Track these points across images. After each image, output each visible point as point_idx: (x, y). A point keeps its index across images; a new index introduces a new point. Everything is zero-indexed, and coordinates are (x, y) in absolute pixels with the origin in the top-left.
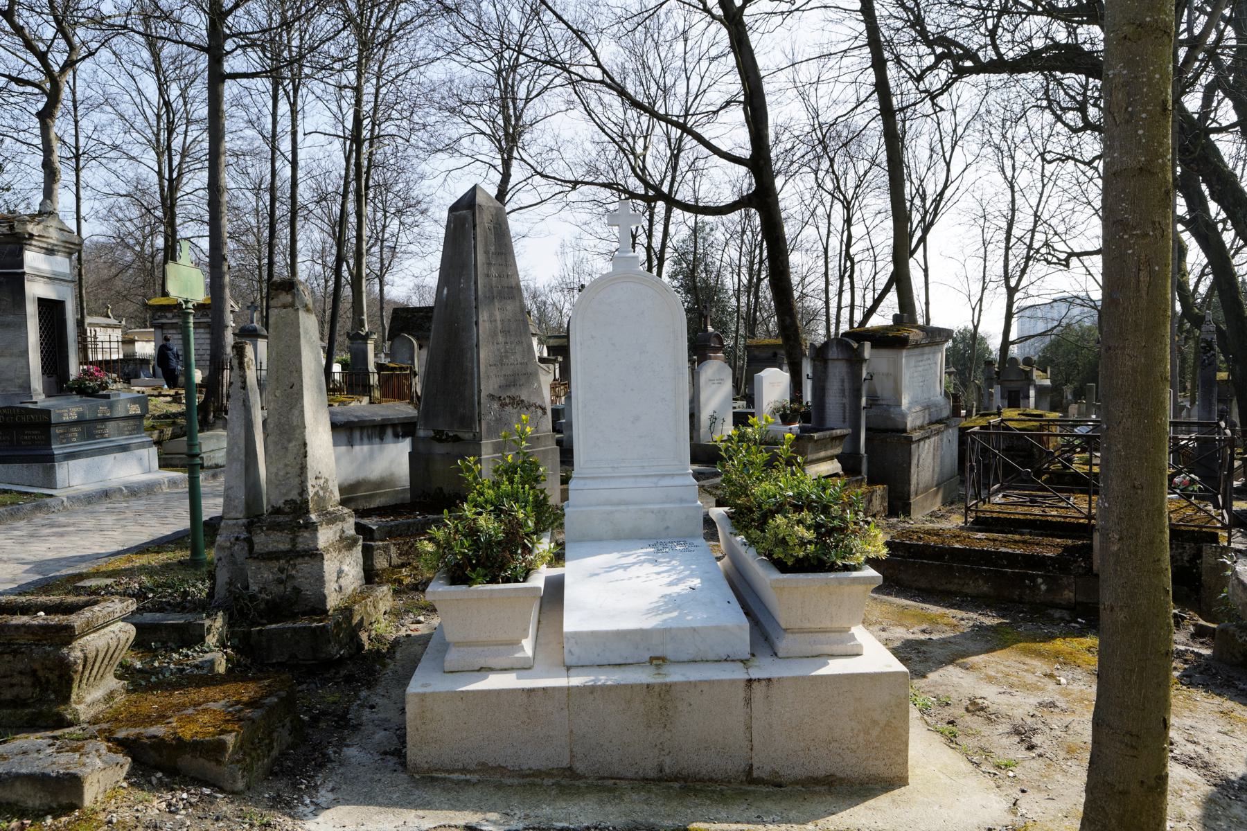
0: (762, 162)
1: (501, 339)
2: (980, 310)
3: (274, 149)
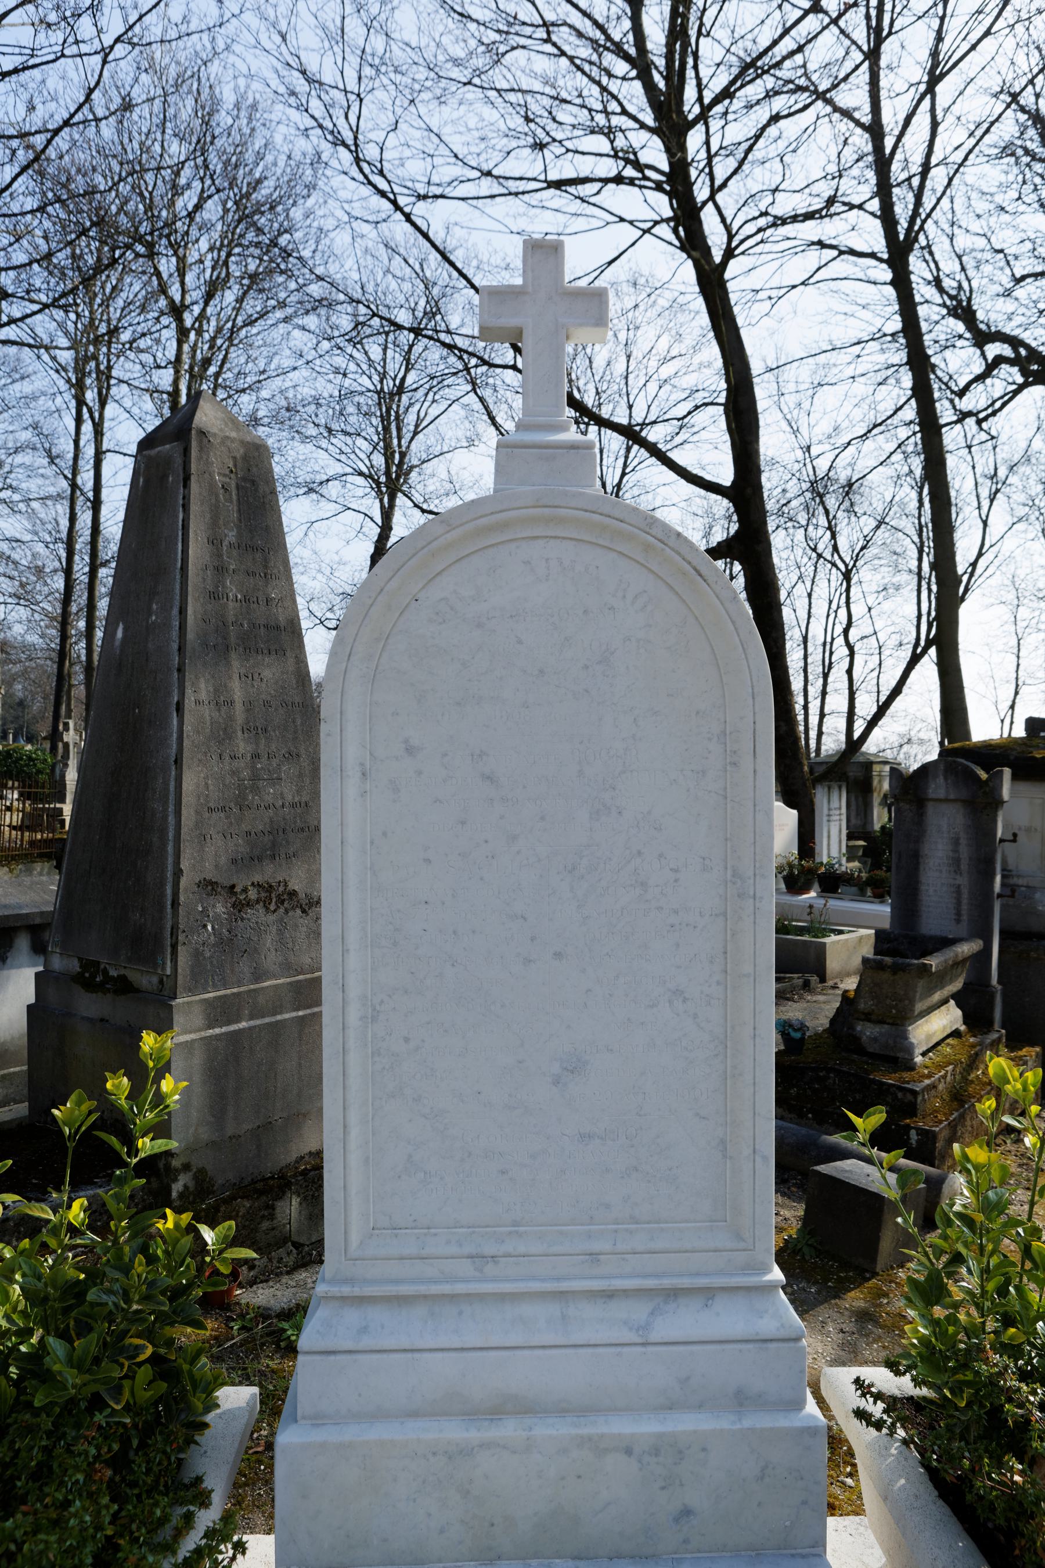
0: (749, 491)
1: (242, 745)
2: (1012, 723)
3: (74, 486)
